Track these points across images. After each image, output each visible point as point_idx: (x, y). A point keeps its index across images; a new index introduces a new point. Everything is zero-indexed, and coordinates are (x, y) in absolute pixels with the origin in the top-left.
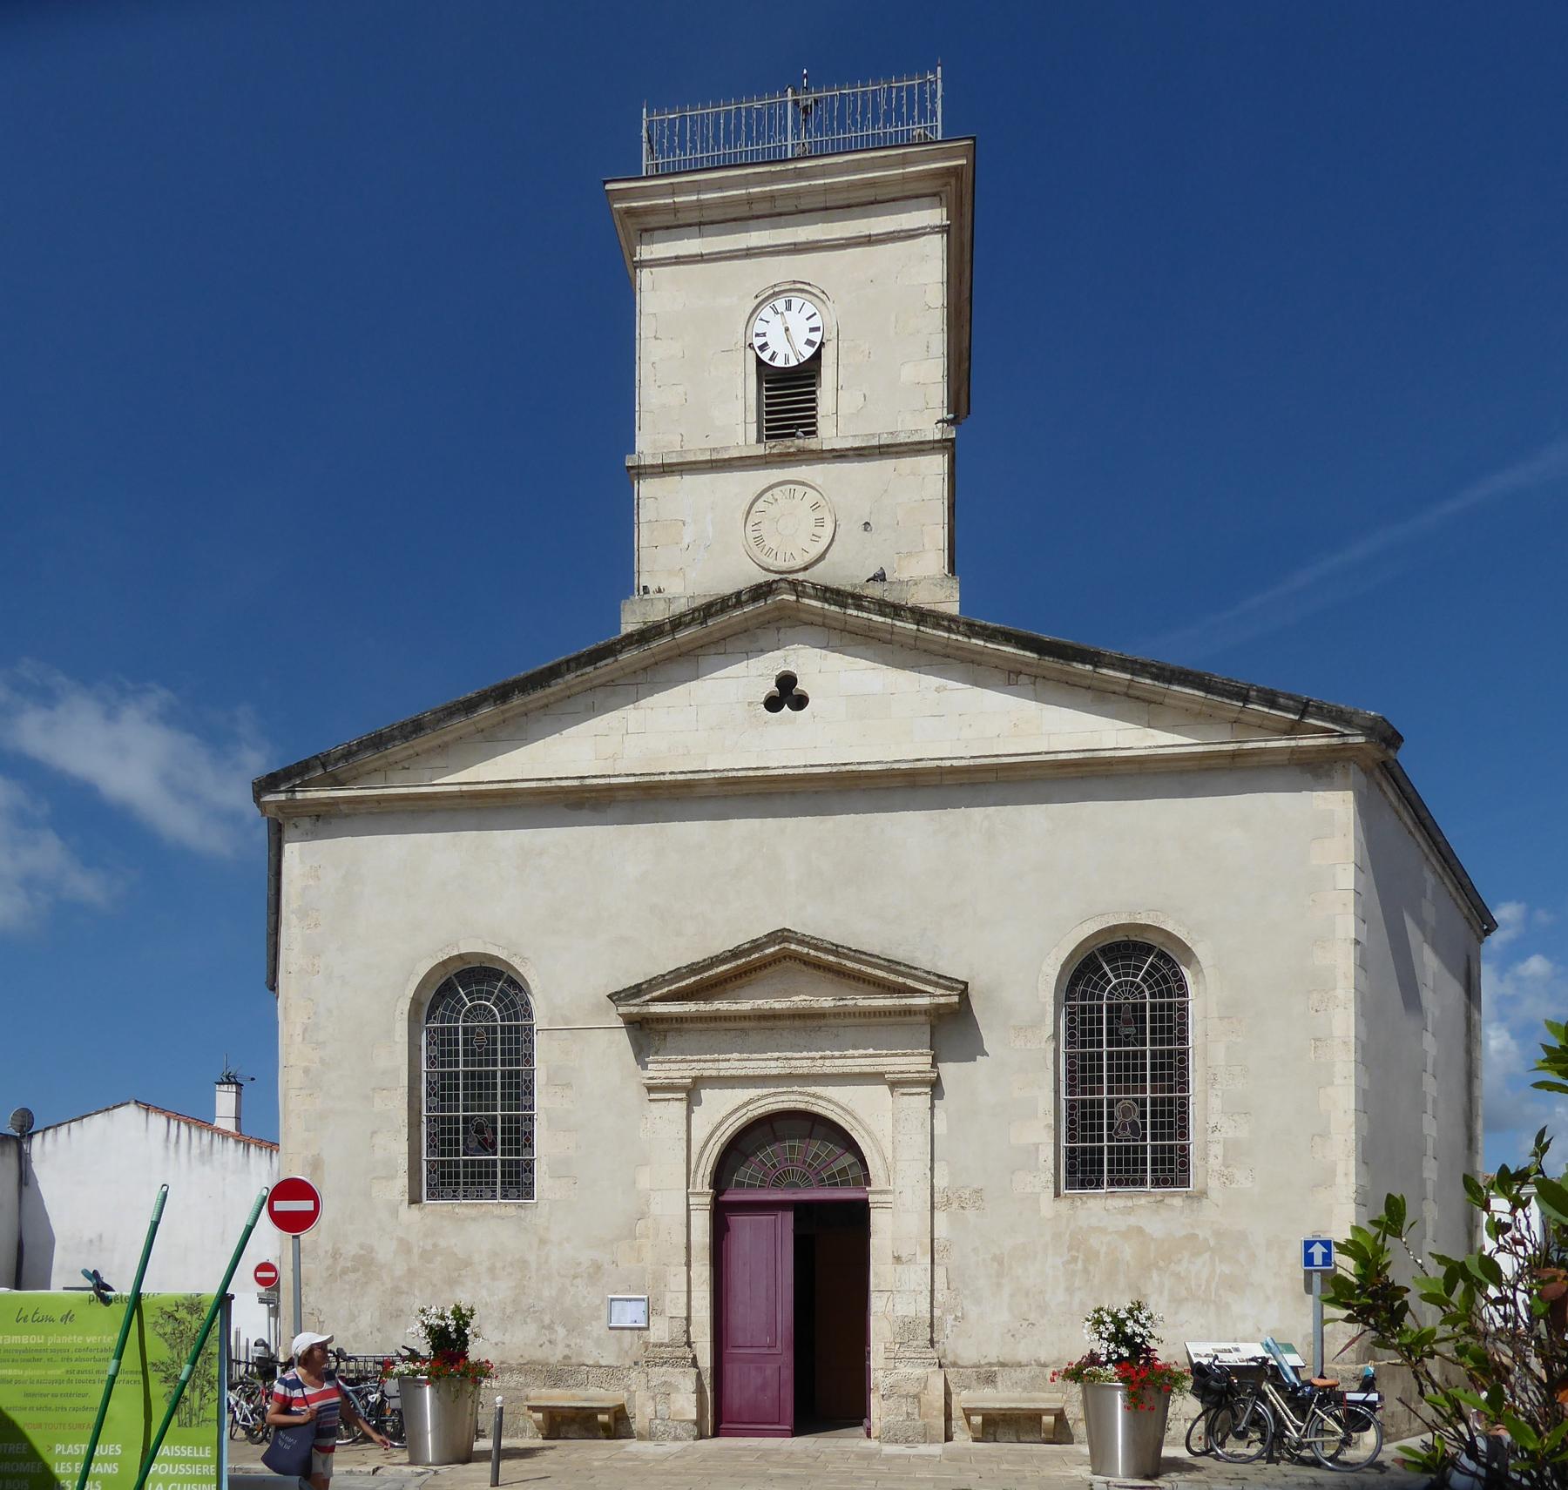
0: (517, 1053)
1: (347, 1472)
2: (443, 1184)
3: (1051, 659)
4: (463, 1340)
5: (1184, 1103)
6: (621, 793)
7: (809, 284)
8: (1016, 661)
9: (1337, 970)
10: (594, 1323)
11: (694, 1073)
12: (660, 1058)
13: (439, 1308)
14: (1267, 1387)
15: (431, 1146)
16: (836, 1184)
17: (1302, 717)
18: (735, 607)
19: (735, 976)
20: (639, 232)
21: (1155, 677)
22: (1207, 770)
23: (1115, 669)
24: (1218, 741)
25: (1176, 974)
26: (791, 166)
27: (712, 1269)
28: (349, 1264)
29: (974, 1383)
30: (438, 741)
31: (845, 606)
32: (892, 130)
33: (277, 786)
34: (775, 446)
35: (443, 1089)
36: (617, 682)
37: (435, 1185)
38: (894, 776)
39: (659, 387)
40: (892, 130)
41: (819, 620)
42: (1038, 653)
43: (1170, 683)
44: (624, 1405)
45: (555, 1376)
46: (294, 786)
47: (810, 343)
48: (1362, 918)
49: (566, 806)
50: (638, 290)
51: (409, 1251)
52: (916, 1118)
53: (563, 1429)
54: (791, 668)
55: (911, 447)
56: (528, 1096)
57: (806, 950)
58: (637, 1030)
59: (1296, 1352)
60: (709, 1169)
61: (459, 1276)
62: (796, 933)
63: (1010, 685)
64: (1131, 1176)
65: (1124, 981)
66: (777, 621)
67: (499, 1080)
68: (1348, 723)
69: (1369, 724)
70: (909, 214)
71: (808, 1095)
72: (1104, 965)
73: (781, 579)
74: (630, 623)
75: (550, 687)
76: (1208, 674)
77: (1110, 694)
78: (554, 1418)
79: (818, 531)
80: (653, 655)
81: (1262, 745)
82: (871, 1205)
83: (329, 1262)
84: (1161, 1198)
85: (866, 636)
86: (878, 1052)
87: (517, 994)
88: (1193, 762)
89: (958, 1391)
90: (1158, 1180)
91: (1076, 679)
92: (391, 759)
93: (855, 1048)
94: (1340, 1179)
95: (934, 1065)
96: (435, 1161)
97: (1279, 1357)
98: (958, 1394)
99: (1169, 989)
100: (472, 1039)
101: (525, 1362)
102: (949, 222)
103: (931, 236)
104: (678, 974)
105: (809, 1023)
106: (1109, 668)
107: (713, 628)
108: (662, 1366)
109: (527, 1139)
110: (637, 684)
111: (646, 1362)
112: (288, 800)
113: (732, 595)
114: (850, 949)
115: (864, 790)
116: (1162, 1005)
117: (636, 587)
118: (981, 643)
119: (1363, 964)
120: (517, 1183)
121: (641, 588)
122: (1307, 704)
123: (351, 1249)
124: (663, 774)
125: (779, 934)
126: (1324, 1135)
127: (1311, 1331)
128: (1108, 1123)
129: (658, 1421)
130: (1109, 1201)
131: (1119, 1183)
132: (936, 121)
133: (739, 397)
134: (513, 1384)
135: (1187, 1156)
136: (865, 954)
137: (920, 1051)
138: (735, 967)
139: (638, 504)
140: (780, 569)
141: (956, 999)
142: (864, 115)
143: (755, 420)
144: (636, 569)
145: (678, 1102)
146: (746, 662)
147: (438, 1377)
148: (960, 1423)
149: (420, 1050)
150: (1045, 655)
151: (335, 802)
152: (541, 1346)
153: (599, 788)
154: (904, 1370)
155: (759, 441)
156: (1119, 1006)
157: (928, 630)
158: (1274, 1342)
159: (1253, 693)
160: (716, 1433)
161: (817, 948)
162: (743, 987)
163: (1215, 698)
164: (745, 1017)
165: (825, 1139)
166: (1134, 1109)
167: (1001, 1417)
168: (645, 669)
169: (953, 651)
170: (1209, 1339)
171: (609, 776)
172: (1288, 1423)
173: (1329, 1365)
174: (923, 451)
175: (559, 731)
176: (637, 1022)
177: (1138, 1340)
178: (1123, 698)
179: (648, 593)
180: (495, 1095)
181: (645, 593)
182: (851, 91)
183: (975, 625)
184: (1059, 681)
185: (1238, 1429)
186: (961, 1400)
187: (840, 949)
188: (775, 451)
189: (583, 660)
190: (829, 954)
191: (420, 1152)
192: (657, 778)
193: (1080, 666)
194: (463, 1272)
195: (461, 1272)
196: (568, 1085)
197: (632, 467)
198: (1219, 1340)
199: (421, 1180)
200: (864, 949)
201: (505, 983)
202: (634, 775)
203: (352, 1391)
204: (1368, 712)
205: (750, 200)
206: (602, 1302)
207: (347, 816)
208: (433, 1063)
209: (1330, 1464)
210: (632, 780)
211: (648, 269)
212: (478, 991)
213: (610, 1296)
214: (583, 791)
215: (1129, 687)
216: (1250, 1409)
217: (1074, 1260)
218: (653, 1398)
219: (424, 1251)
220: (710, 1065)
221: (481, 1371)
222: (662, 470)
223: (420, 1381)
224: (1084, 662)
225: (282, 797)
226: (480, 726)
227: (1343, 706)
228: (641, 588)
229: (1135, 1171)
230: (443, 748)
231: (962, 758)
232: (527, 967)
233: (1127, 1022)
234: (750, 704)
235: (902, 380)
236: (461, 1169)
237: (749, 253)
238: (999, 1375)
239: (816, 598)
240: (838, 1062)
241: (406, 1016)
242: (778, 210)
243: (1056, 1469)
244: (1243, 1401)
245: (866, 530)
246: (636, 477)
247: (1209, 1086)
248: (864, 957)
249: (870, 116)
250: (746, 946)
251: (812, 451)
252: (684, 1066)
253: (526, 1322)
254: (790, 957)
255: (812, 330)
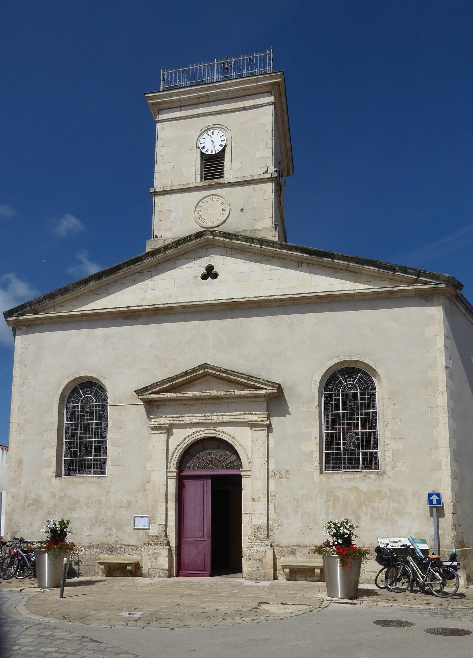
0: (101, 415)
1: (10, 591)
2: (70, 469)
3: (314, 257)
4: (64, 534)
5: (375, 434)
6: (144, 312)
7: (221, 125)
8: (301, 258)
9: (438, 379)
10: (127, 527)
11: (170, 422)
12: (156, 416)
13: (56, 519)
14: (409, 558)
15: (66, 454)
16: (229, 468)
17: (418, 277)
18: (189, 241)
19: (187, 383)
20: (158, 111)
21: (357, 263)
22: (380, 299)
23: (340, 260)
24: (385, 287)
25: (370, 380)
26: (214, 85)
27: (177, 504)
28: (31, 502)
29: (286, 554)
30: (75, 295)
31: (232, 239)
32: (254, 71)
33: (13, 314)
34: (207, 182)
35: (72, 431)
36: (143, 271)
37: (67, 469)
38: (252, 303)
39: (164, 163)
40: (254, 71)
41: (222, 245)
42: (309, 254)
43: (363, 265)
44: (139, 562)
45: (112, 549)
46: (19, 314)
47: (221, 145)
48: (449, 357)
49: (123, 318)
50: (157, 131)
51: (55, 496)
52: (261, 440)
53: (114, 572)
54: (212, 263)
55: (260, 180)
56: (105, 433)
57: (214, 372)
58: (148, 405)
59: (426, 543)
60: (176, 462)
61: (74, 507)
62: (210, 365)
63: (299, 267)
64: (353, 465)
65: (349, 384)
66: (207, 246)
67: (94, 426)
68: (438, 279)
69: (447, 279)
70: (259, 99)
71: (217, 431)
72: (340, 377)
73: (207, 230)
74: (149, 248)
75: (117, 273)
76: (377, 261)
77: (340, 270)
78: (110, 567)
79: (223, 212)
80: (158, 260)
81: (402, 288)
82: (242, 477)
83: (23, 501)
84: (366, 474)
85: (241, 250)
86: (245, 413)
87: (102, 392)
88: (374, 296)
89: (280, 558)
90: (365, 466)
91: (325, 264)
92: (57, 303)
93: (236, 411)
94: (444, 467)
95: (268, 418)
96: (68, 460)
97: (415, 545)
98: (280, 559)
99: (368, 387)
100: (84, 410)
101: (99, 543)
102: (274, 101)
103: (268, 106)
104: (163, 382)
105: (217, 401)
106: (338, 260)
107: (181, 250)
108: (154, 545)
109: (104, 450)
110: (152, 271)
111: (148, 543)
112: (16, 319)
113: (188, 236)
114: (232, 371)
115: (240, 309)
116: (365, 394)
117: (153, 235)
118: (286, 251)
119: (450, 376)
120: (100, 468)
121: (154, 236)
122: (420, 272)
123: (32, 496)
124: (160, 304)
125: (203, 365)
126: (436, 448)
127: (433, 533)
128: (343, 443)
129: (152, 569)
130: (343, 475)
131: (348, 468)
132: (270, 67)
133: (194, 166)
134: (94, 553)
135: (377, 456)
136: (238, 373)
137: (263, 412)
138: (186, 379)
139: (154, 206)
140: (208, 227)
141: (276, 391)
142: (243, 66)
143: (200, 173)
144: (153, 229)
145: (163, 434)
146: (194, 262)
147: (49, 550)
148: (280, 572)
149: (64, 415)
150: (312, 255)
151: (35, 319)
152: (106, 536)
153: (135, 311)
154: (256, 548)
155: (201, 180)
156: (347, 394)
157: (265, 247)
158: (412, 538)
159: (397, 268)
160: (178, 575)
161: (219, 371)
162: (190, 387)
163: (382, 270)
164: (190, 399)
165: (225, 449)
166: (354, 436)
167: (298, 569)
168: (155, 266)
169: (276, 255)
170: (388, 536)
171: (139, 306)
172: (419, 575)
173: (442, 549)
174: (264, 182)
175: (121, 290)
176: (148, 402)
177: (346, 536)
178: (345, 271)
179: (157, 237)
180: (92, 432)
181: (156, 238)
182: (238, 59)
183: (283, 245)
184: (318, 265)
185: (397, 577)
186: (281, 561)
187: (228, 371)
188: (207, 184)
189: (130, 263)
190: (224, 373)
191: (62, 456)
192: (157, 306)
193: (326, 259)
194: (76, 505)
195: (75, 505)
196: (120, 428)
197: (152, 192)
198: (393, 537)
199: (61, 467)
200: (240, 371)
201: (98, 387)
202: (148, 305)
203: (25, 556)
204: (446, 274)
205: (199, 97)
206: (131, 518)
207: (39, 325)
208: (68, 420)
209: (436, 593)
210: (147, 307)
211: (161, 123)
212: (87, 391)
213: (134, 515)
214: (129, 312)
215: (347, 267)
216: (402, 568)
217: (329, 500)
218: (150, 559)
219: (61, 497)
220: (176, 419)
221: (71, 547)
222: (163, 193)
223: (42, 551)
224: (327, 258)
225: (14, 318)
226: (91, 289)
227: (435, 272)
228: (154, 236)
229: (355, 463)
230: (77, 298)
231: (278, 295)
232: (106, 381)
233: (350, 400)
234: (195, 277)
235: (256, 156)
236: (78, 463)
237: (199, 116)
238: (297, 551)
239: (220, 236)
240: (228, 417)
241: (58, 401)
242: (210, 100)
243: (313, 594)
244: (399, 564)
245: (242, 211)
246: (154, 196)
247: (385, 427)
248: (238, 374)
249: (245, 67)
250: (190, 371)
251: (221, 184)
252: (166, 419)
253: (100, 527)
254: (209, 375)
255: (222, 141)
